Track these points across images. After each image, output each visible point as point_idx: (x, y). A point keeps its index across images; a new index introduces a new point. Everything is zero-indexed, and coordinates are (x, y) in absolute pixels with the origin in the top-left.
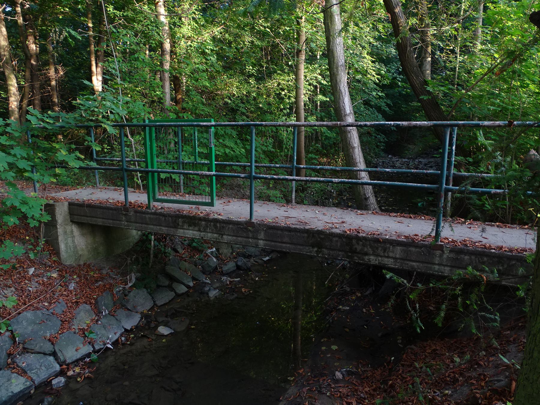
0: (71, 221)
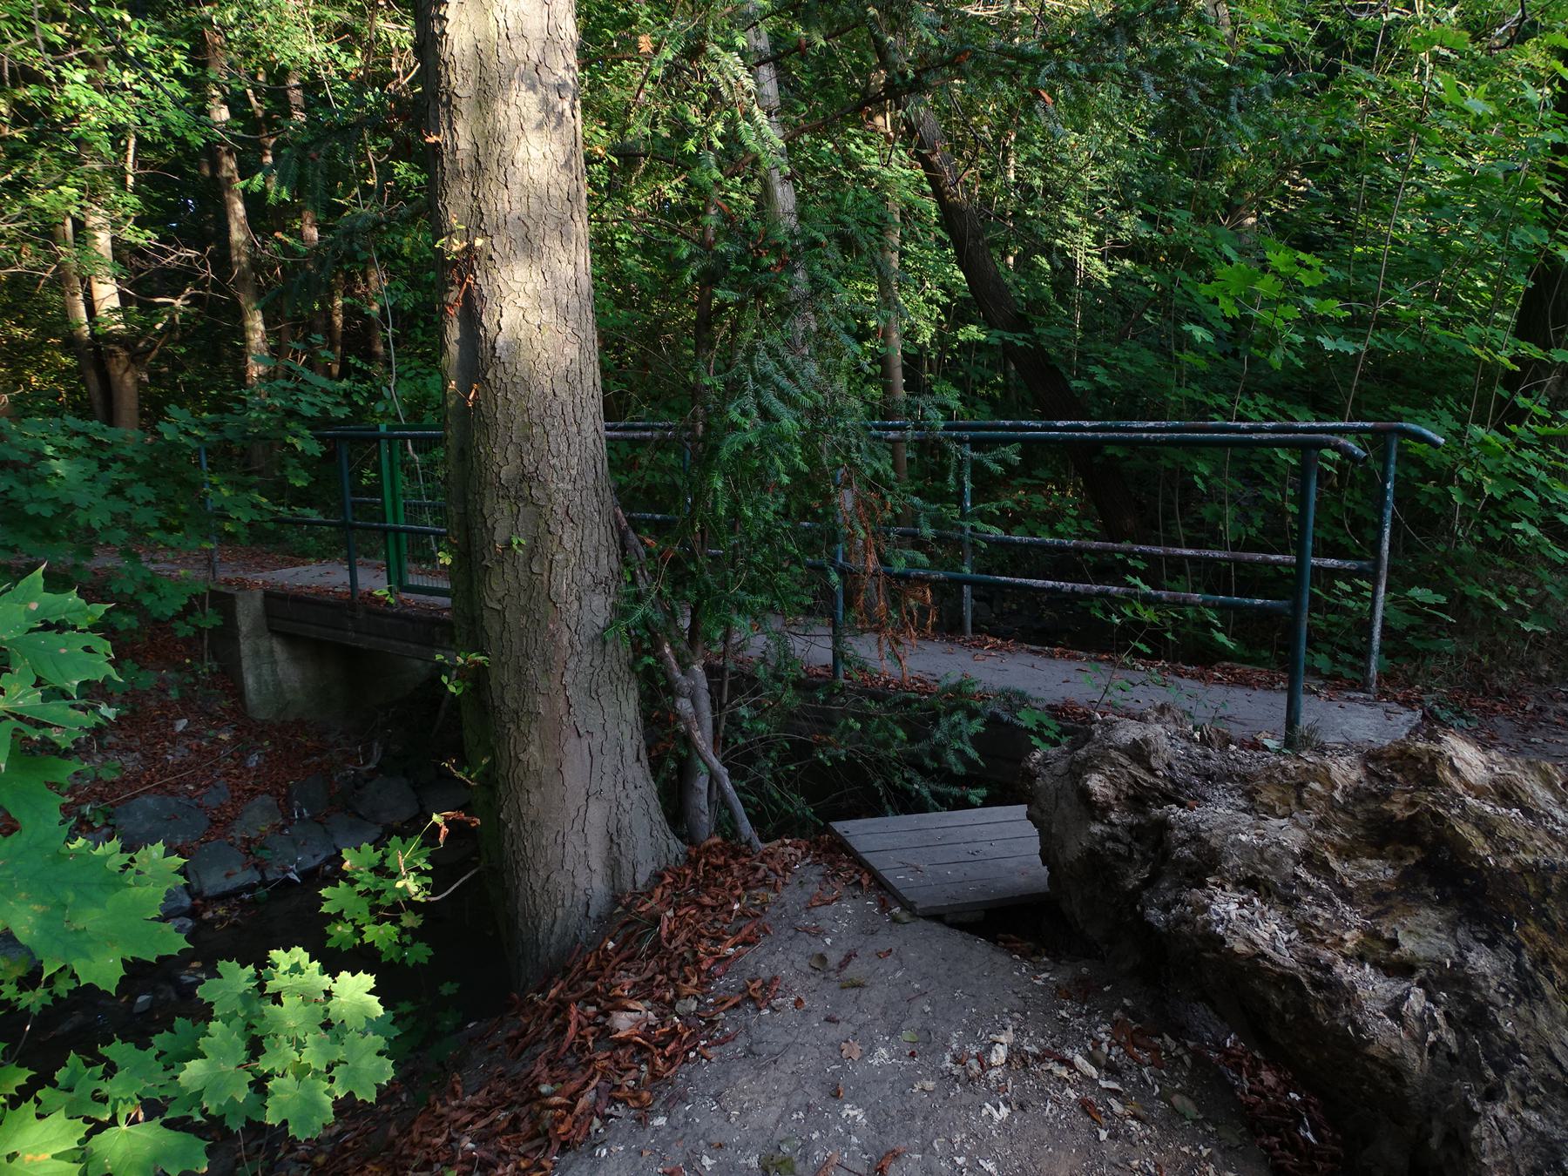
0: (270, 630)
